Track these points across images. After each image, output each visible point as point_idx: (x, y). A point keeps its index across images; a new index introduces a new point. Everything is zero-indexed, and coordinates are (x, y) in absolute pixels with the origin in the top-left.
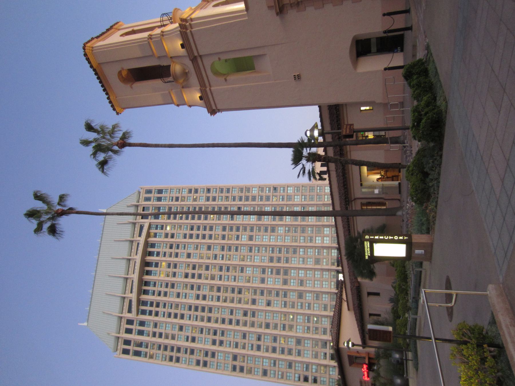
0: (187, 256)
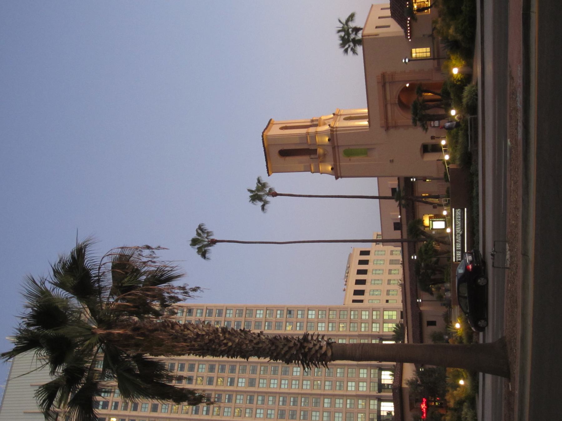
0: (151, 408)
